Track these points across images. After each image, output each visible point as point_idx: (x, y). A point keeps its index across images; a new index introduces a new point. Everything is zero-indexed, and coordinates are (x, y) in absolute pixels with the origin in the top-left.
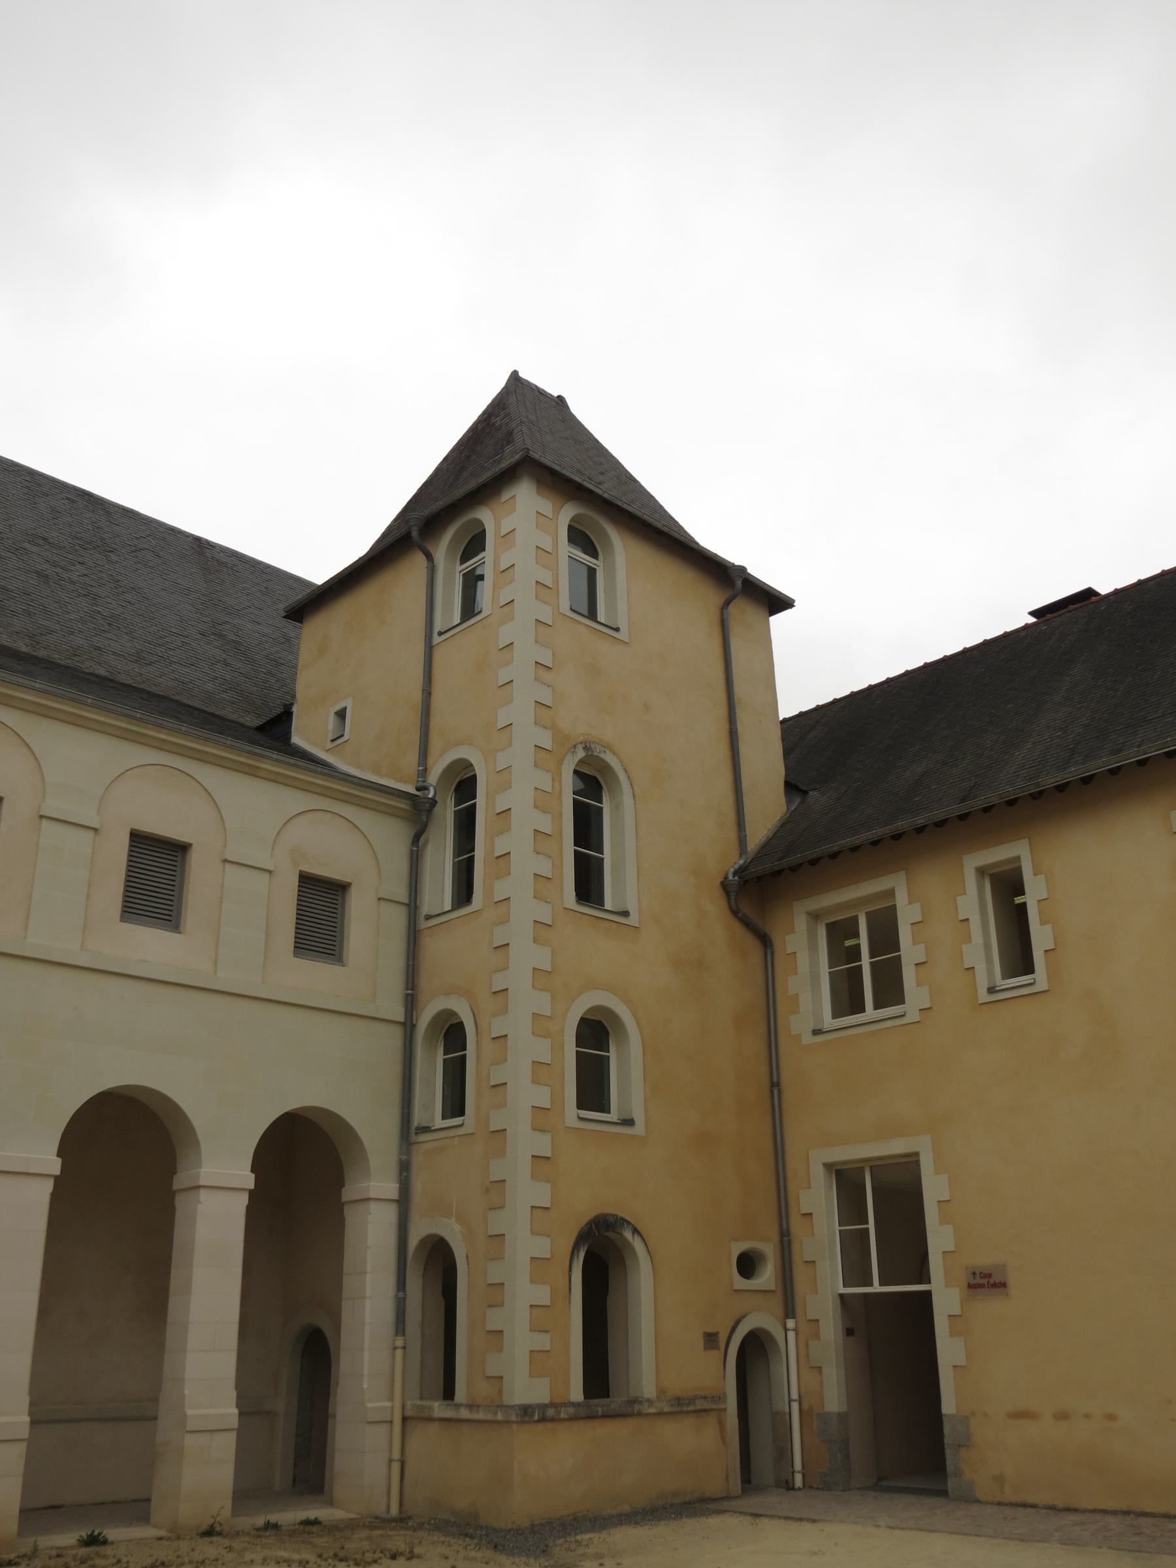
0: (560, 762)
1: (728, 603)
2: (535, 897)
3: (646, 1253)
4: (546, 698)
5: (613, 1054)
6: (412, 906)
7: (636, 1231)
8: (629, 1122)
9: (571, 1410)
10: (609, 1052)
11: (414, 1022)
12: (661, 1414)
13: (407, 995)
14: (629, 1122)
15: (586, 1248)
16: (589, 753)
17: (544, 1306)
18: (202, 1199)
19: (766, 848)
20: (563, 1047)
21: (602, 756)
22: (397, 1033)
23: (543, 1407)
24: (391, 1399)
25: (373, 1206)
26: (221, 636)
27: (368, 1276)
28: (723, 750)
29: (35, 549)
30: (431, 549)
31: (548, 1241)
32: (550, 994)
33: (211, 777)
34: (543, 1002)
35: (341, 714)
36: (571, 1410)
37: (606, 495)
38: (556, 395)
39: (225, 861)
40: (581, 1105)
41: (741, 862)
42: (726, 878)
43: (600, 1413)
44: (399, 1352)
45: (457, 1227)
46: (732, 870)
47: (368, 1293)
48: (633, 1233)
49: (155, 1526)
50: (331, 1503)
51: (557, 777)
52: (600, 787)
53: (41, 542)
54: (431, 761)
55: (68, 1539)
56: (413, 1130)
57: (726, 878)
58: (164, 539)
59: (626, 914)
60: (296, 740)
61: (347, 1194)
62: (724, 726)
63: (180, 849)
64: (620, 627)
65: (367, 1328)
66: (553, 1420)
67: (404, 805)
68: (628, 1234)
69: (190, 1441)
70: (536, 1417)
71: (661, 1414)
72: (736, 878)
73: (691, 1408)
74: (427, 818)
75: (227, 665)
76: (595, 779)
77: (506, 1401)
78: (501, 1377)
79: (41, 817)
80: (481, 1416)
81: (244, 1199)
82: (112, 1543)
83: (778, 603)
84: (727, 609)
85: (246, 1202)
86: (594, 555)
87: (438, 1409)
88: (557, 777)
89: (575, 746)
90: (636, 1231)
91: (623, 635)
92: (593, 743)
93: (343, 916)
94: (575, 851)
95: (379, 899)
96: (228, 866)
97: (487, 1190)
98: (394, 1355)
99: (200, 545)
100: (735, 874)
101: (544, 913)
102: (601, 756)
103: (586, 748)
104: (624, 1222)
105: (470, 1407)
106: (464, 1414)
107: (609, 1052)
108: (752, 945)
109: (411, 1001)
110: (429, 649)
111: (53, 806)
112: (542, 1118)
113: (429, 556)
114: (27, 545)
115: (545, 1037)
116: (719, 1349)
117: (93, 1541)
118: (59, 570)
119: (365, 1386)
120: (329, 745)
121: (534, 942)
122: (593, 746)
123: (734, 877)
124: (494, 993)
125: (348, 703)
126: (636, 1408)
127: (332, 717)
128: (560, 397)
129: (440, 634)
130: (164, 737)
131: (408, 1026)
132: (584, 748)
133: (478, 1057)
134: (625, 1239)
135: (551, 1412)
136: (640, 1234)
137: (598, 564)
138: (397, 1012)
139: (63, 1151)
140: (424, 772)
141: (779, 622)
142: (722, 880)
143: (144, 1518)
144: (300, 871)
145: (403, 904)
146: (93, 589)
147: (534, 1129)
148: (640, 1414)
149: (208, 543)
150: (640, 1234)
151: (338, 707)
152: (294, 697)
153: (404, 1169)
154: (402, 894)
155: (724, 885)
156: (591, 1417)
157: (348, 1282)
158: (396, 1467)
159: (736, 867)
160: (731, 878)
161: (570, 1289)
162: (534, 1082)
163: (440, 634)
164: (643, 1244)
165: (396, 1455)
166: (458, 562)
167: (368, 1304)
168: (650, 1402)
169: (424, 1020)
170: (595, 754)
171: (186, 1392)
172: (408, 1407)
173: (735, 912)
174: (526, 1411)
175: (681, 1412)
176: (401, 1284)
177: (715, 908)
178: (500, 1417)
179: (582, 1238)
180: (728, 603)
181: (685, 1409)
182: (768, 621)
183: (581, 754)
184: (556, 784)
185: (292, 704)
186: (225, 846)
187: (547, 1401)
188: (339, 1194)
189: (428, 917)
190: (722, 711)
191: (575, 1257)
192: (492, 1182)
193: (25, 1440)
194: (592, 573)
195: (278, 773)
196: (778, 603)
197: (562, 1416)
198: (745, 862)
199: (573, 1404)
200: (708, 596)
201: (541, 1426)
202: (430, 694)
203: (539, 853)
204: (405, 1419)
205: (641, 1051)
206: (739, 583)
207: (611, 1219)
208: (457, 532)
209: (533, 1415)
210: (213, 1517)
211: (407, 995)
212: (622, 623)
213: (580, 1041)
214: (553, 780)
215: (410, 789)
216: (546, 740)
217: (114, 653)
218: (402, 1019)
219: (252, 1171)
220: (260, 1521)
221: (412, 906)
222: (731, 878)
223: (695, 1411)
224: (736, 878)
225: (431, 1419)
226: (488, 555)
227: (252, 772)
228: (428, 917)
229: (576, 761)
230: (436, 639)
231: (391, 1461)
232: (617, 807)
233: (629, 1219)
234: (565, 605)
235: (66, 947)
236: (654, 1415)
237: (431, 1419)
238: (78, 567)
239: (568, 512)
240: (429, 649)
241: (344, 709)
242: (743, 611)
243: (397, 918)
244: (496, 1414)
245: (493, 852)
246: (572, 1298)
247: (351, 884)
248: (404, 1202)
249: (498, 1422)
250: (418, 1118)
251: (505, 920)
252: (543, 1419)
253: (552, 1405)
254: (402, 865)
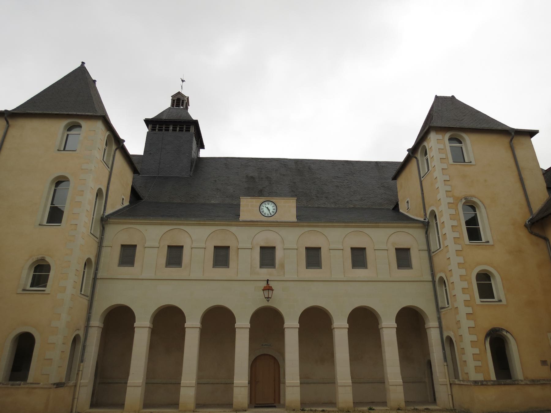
0: (457, 205)
1: (511, 140)
2: (455, 244)
3: (512, 337)
4: (449, 188)
5: (492, 282)
6: (429, 250)
7: (507, 332)
8: (500, 301)
9: (492, 382)
10: (491, 281)
11: (435, 280)
12: (527, 384)
13: (431, 274)
14: (500, 301)
15: (489, 337)
16: (467, 200)
17: (478, 354)
18: (383, 330)
19: (541, 211)
20: (472, 283)
21: (472, 199)
22: (430, 285)
23: (482, 381)
24: (446, 379)
25: (432, 329)
26: (384, 186)
27: (434, 347)
28: (518, 185)
29: (335, 180)
30: (416, 156)
31: (476, 336)
32: (465, 269)
33: (367, 231)
34: (463, 272)
35: (408, 202)
36: (492, 382)
37: (458, 127)
38: (451, 96)
39: (375, 250)
40: (481, 297)
41: (531, 217)
42: (526, 223)
43: (503, 383)
44: (446, 367)
45: (452, 333)
46: (527, 221)
47: (434, 351)
48: (506, 333)
49: (388, 407)
50: (437, 405)
51: (457, 209)
52: (475, 208)
53: (336, 178)
54: (426, 211)
55: (365, 409)
56: (439, 309)
57: (526, 223)
58: (367, 166)
59: (488, 242)
60: (401, 211)
61: (426, 326)
62: (517, 178)
63: (364, 249)
64: (471, 161)
65: (436, 361)
66: (485, 385)
67: (421, 225)
68: (505, 333)
69: (391, 388)
70: (480, 384)
71: (527, 384)
72: (529, 223)
73: (539, 383)
74: (428, 227)
75: (385, 194)
76: (472, 206)
77: (470, 379)
78: (468, 373)
79: (330, 249)
80: (465, 383)
81: (395, 330)
82: (375, 410)
83: (532, 133)
84: (511, 142)
85: (396, 330)
86: (461, 143)
87: (457, 382)
88: (457, 209)
89: (461, 200)
90: (507, 332)
91: (473, 163)
92: (468, 197)
93: (410, 256)
94: (467, 227)
95: (419, 250)
96: (376, 251)
97: (457, 323)
98: (444, 367)
99: (377, 163)
100: (529, 222)
101: (459, 247)
102: (471, 199)
103: (465, 199)
104: (502, 329)
105: (463, 381)
106: (462, 383)
107: (491, 281)
108: (541, 242)
109: (433, 275)
110: (421, 182)
111: (332, 246)
112: (467, 303)
113: (416, 158)
114: (333, 180)
115: (465, 281)
116: (548, 365)
117: (370, 409)
118: (341, 184)
119: (438, 375)
120: (407, 211)
121: (457, 256)
122: (468, 198)
123: (528, 222)
124: (449, 271)
125: (408, 199)
126: (516, 382)
127: (406, 203)
128: (452, 96)
129: (423, 177)
130: (353, 225)
131: (434, 282)
132: (465, 199)
133: (449, 288)
134: (504, 334)
135: (485, 383)
136: (509, 332)
137: (463, 145)
138: (430, 278)
139: (349, 322)
140: (425, 215)
141: (534, 139)
142: (524, 224)
143: (386, 406)
144: (395, 248)
145: (427, 250)
146: (350, 185)
147: (465, 306)
148: (518, 384)
149: (379, 162)
150: (509, 332)
151: (407, 201)
152: (398, 200)
153: (439, 319)
154: (425, 247)
155: (526, 226)
156: (499, 384)
157: (430, 348)
158: (450, 396)
159: (529, 219)
160: (527, 223)
161: (486, 349)
162: (463, 293)
163: (423, 177)
164: (511, 335)
165: (450, 393)
166: (424, 157)
167: (435, 354)
168: (522, 381)
169: (437, 279)
170: (469, 199)
171: (388, 376)
172: (451, 381)
173: (531, 233)
174: (476, 383)
175: (535, 384)
176: (444, 349)
177: (524, 234)
178: (469, 384)
179: (488, 335)
180: (511, 140)
181: (536, 383)
182: (531, 140)
183: (464, 201)
184: (457, 211)
185: (398, 202)
186: (374, 246)
187: (483, 379)
188: (378, 327)
189: (433, 252)
190: (516, 173)
191: (486, 340)
192: (458, 321)
193: (351, 386)
194: (462, 147)
195: (384, 226)
196: (532, 133)
197: (489, 384)
198: (533, 217)
199: (492, 381)
200: (505, 140)
201: (482, 387)
202: (423, 194)
203: (454, 232)
204: (451, 384)
205: (501, 280)
206: (513, 133)
207: (498, 329)
208: (421, 150)
209: (478, 383)
210: (398, 405)
211: (431, 274)
212: (472, 160)
213: (477, 280)
214: (456, 211)
215: (422, 219)
216: (451, 200)
217: (355, 200)
218: (431, 280)
219: (396, 323)
220: (413, 408)
221: (429, 250)
222: (527, 223)
223: (540, 384)
224: (529, 223)
225: (456, 384)
226: (428, 155)
227: (378, 227)
228: (433, 252)
229: (462, 203)
230: (422, 179)
231: (449, 395)
232: (480, 212)
233: (504, 328)
234: (451, 161)
235: (341, 277)
236: (524, 384)
237: (456, 384)
238: (346, 181)
239: (447, 135)
240: (421, 182)
241: (408, 201)
242: (518, 141)
243: (425, 254)
244: (468, 383)
245: (442, 233)
246: (487, 351)
247: (410, 248)
248: (441, 327)
249: (468, 385)
250: (440, 305)
251: (448, 251)
252: (482, 385)
253: (485, 381)
254: (424, 240)
